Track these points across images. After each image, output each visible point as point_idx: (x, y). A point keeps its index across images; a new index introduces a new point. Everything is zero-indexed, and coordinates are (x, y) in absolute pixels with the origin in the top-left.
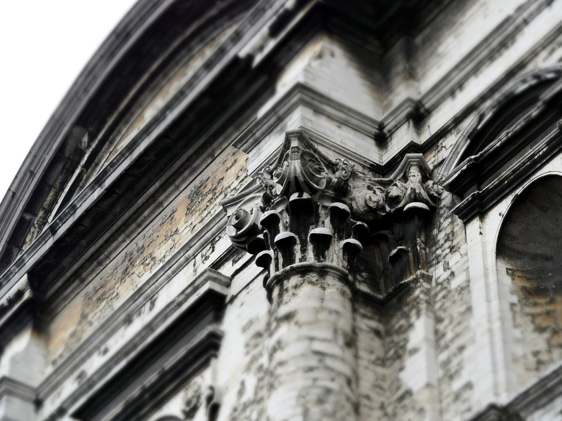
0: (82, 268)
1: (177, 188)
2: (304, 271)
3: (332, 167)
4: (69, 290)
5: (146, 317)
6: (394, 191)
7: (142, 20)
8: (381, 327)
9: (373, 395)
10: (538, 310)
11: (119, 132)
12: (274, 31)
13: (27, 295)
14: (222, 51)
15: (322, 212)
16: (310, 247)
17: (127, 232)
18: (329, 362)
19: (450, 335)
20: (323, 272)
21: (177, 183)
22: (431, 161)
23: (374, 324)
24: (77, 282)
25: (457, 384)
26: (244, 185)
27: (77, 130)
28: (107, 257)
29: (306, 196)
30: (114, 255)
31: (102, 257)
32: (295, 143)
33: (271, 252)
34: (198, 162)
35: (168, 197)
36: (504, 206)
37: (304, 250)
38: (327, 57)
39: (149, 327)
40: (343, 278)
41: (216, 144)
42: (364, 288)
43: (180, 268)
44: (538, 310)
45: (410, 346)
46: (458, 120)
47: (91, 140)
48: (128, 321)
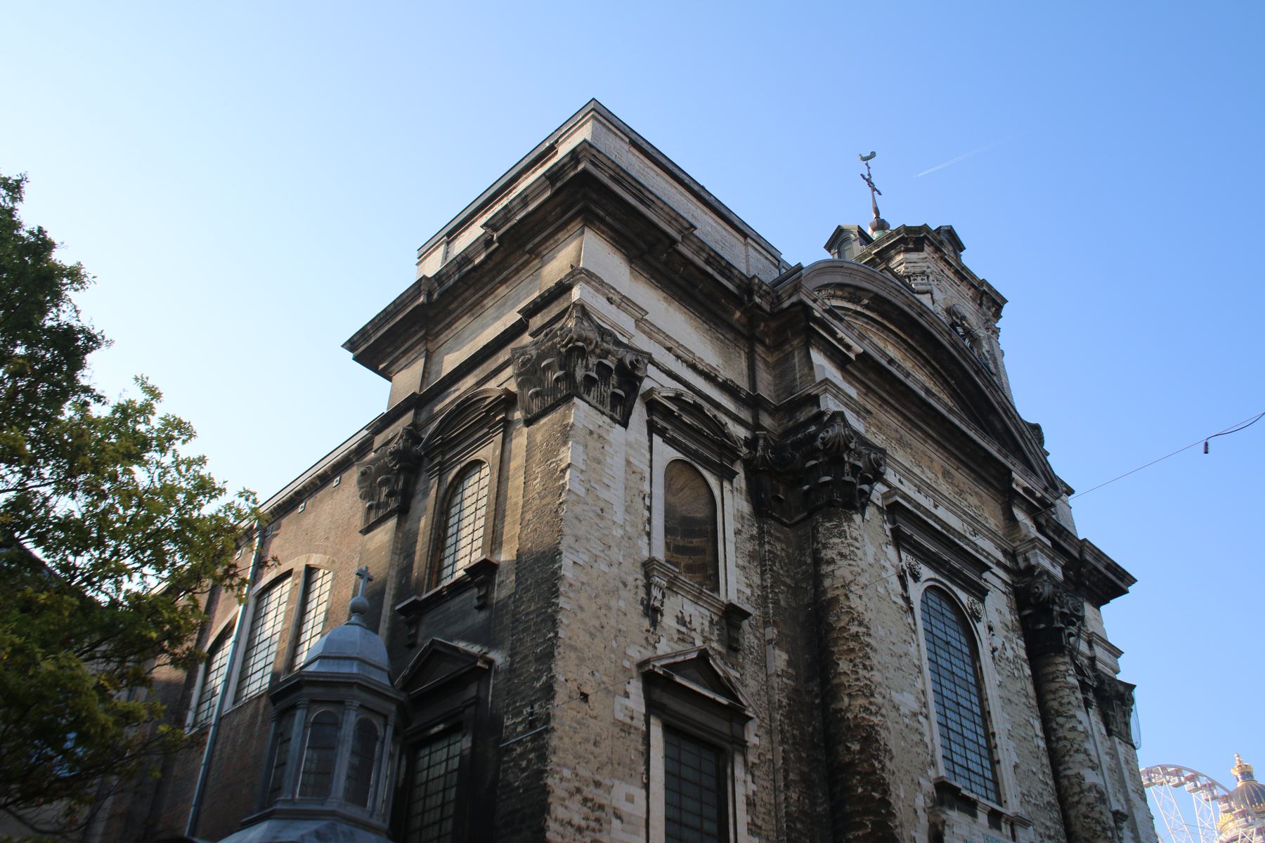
0: (875, 392)
1: (937, 451)
4: (857, 385)
5: (927, 503)
11: (980, 484)
12: (1025, 489)
17: (905, 422)
21: (940, 450)
24: (864, 390)
26: (1102, 743)
28: (886, 411)
30: (888, 415)
31: (886, 407)
34: (953, 460)
35: (931, 446)
41: (964, 469)
43: (711, 276)
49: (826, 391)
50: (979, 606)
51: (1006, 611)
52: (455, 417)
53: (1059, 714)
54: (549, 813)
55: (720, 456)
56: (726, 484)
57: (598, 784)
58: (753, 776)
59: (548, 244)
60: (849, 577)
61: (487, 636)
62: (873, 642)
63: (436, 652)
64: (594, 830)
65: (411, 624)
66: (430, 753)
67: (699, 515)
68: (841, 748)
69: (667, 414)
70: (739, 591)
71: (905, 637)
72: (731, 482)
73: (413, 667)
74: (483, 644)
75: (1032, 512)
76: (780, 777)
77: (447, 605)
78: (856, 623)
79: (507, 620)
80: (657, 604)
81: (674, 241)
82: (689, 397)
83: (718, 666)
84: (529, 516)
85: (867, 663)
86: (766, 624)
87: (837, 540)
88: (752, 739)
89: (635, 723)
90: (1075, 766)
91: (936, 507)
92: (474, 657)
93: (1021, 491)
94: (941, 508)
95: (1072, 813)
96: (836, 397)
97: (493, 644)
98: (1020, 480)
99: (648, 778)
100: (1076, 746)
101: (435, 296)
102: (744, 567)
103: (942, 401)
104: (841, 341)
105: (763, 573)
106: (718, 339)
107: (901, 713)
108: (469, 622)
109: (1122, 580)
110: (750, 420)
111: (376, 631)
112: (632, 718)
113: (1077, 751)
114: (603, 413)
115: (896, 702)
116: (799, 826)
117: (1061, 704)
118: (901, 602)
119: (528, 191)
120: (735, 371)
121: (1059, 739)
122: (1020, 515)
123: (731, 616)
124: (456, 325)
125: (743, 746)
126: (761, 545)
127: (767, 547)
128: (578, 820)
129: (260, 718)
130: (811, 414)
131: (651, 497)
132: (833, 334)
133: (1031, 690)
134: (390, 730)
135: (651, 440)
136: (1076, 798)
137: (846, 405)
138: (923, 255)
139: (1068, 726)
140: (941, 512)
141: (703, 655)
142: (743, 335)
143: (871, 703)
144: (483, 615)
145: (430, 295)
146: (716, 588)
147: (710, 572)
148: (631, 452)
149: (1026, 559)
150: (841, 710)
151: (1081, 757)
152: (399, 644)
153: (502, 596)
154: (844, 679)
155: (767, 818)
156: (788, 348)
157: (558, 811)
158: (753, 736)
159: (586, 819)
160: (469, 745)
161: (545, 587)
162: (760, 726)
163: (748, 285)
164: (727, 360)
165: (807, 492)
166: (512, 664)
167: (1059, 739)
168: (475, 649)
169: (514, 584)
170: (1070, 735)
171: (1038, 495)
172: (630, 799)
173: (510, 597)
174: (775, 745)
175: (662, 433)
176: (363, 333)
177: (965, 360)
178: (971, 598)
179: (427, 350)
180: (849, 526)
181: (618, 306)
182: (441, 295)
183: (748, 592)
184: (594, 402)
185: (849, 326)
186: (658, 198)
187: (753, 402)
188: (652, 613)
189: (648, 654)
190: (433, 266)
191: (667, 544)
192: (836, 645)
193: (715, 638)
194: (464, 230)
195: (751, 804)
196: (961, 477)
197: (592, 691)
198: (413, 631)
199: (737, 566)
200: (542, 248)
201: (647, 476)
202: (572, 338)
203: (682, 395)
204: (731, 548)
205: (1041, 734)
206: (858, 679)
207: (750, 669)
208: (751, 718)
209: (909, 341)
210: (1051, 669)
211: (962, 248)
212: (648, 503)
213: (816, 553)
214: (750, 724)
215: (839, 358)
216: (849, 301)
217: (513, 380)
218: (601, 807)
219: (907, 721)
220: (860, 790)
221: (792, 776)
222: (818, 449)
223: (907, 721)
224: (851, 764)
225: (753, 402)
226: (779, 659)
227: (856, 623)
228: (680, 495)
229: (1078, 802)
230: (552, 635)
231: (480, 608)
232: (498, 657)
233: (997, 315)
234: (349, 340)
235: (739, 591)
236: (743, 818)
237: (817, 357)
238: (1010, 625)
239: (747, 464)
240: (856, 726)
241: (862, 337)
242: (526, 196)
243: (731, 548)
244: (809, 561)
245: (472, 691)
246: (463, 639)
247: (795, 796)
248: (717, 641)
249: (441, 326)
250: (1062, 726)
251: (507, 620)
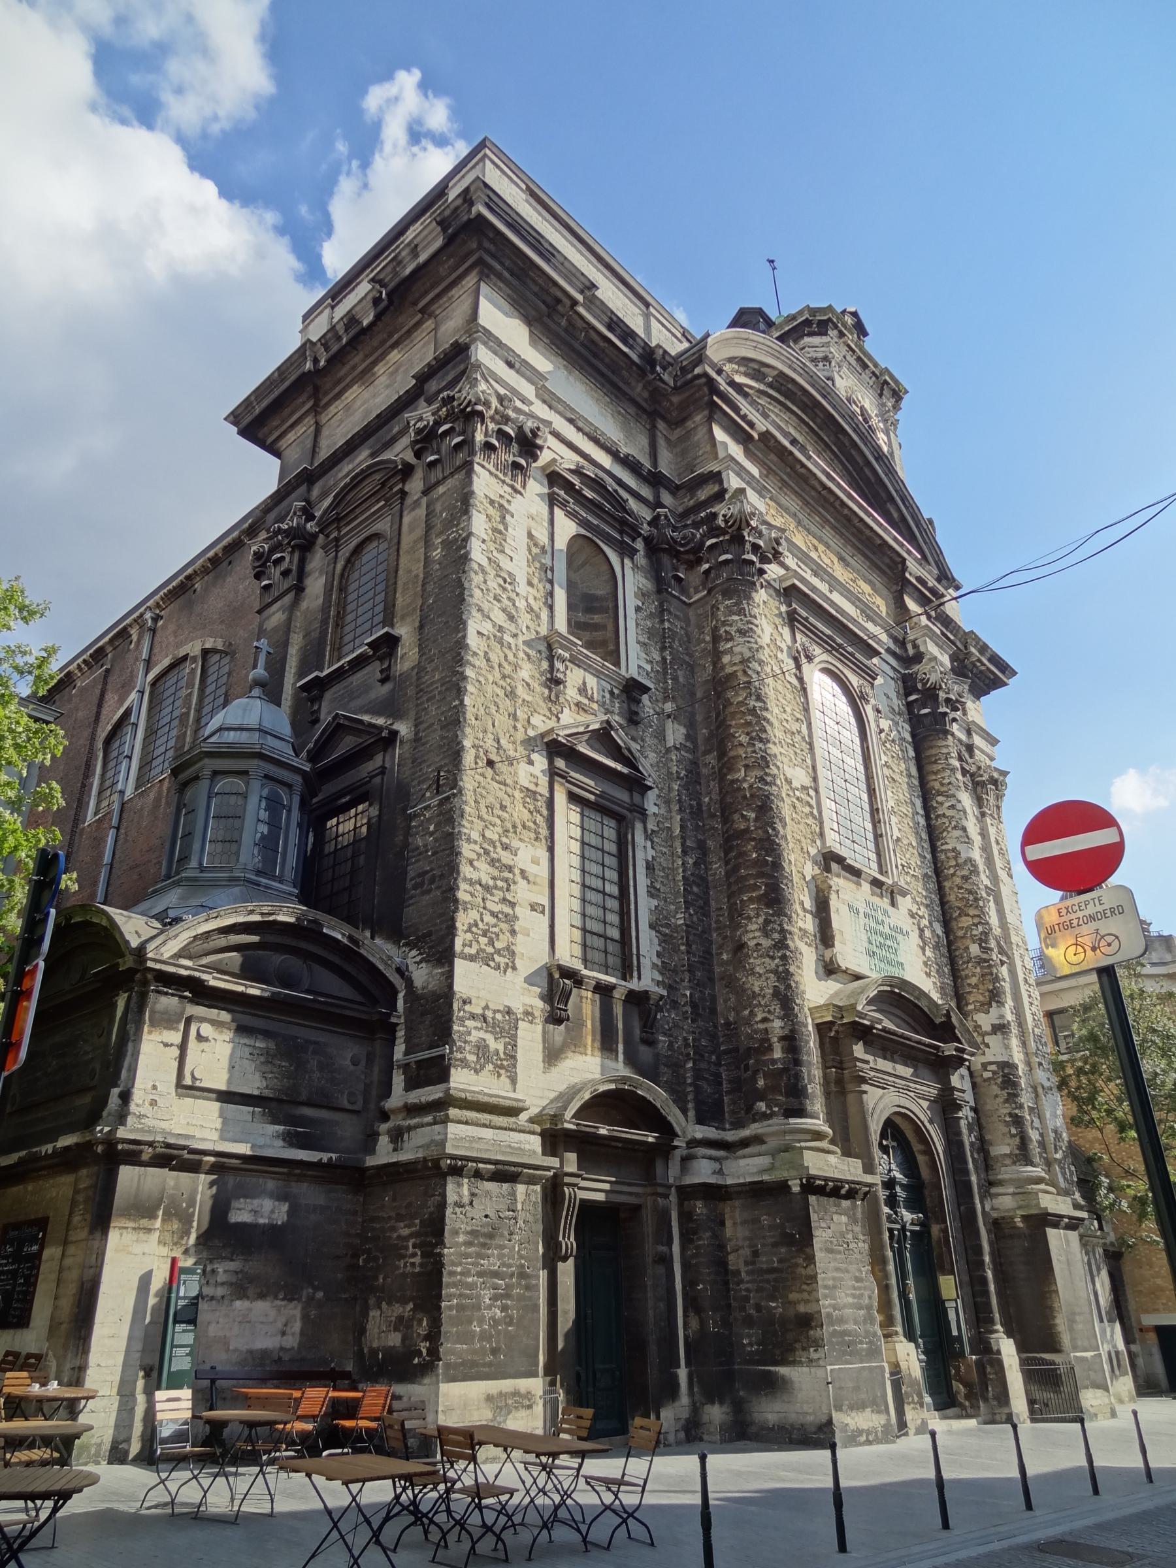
5: (823, 587)
12: (919, 579)
49: (728, 468)
50: (868, 690)
51: (893, 695)
52: (351, 490)
53: (939, 793)
54: (458, 873)
55: (621, 532)
56: (627, 561)
57: (506, 847)
58: (652, 842)
59: (441, 302)
60: (748, 654)
61: (391, 707)
62: (769, 716)
63: (339, 726)
64: (501, 889)
65: (313, 700)
66: (338, 824)
67: (600, 592)
68: (736, 817)
69: (569, 487)
70: (639, 667)
71: (799, 716)
72: (632, 559)
73: (317, 741)
74: (388, 717)
75: (923, 601)
76: (678, 844)
77: (350, 679)
78: (754, 697)
79: (411, 691)
80: (560, 676)
81: (575, 302)
82: (590, 472)
83: (620, 737)
84: (429, 588)
85: (764, 736)
86: (666, 699)
87: (736, 618)
88: (651, 809)
89: (539, 789)
90: (951, 841)
91: (831, 592)
92: (380, 729)
93: (914, 581)
94: (835, 593)
95: (947, 884)
96: (738, 475)
97: (397, 715)
98: (914, 569)
99: (553, 842)
100: (953, 823)
101: (322, 363)
102: (645, 644)
103: (841, 487)
104: (744, 417)
105: (663, 649)
106: (619, 413)
107: (793, 786)
108: (373, 695)
109: (1003, 672)
110: (651, 498)
111: (279, 704)
112: (537, 785)
113: (955, 827)
114: (504, 482)
115: (789, 776)
116: (695, 889)
117: (942, 785)
118: (795, 682)
119: (418, 239)
120: (635, 448)
121: (938, 816)
122: (912, 606)
123: (632, 690)
124: (346, 395)
125: (643, 813)
126: (662, 621)
127: (667, 625)
128: (486, 879)
129: (163, 800)
130: (712, 492)
131: (552, 570)
132: (737, 410)
133: (914, 771)
134: (296, 799)
135: (552, 513)
136: (952, 871)
137: (748, 483)
138: (825, 339)
139: (947, 804)
140: (836, 597)
141: (607, 727)
142: (644, 410)
143: (766, 774)
144: (388, 687)
145: (316, 361)
146: (617, 664)
147: (612, 647)
148: (533, 524)
149: (915, 646)
150: (737, 780)
151: (957, 833)
152: (303, 719)
153: (405, 669)
154: (741, 751)
155: (665, 881)
156: (690, 424)
157: (466, 870)
158: (651, 804)
159: (494, 878)
160: (377, 813)
161: (448, 656)
162: (659, 796)
163: (650, 356)
164: (628, 434)
165: (707, 572)
166: (416, 734)
167: (938, 816)
168: (380, 721)
169: (417, 656)
170: (949, 813)
171: (930, 584)
172: (535, 861)
173: (413, 668)
174: (673, 814)
175: (563, 505)
176: (247, 403)
177: (866, 444)
178: (861, 682)
179: (317, 423)
180: (748, 604)
181: (518, 372)
182: (328, 361)
183: (648, 667)
184: (493, 470)
185: (753, 403)
186: (559, 252)
187: (655, 480)
188: (554, 682)
189: (552, 724)
190: (318, 330)
191: (569, 621)
192: (733, 718)
193: (617, 711)
194: (349, 293)
195: (650, 867)
196: (856, 561)
197: (499, 759)
198: (316, 708)
199: (638, 642)
200: (436, 305)
201: (549, 549)
202: (470, 401)
203: (583, 467)
204: (631, 625)
205: (921, 812)
206: (754, 752)
207: (650, 741)
208: (650, 788)
209: (811, 423)
210: (933, 752)
211: (865, 334)
212: (550, 576)
213: (715, 630)
214: (649, 793)
215: (742, 436)
216: (753, 378)
217: (410, 450)
218: (510, 869)
219: (797, 793)
220: (754, 855)
221: (689, 843)
222: (719, 528)
223: (797, 793)
224: (747, 831)
225: (655, 480)
226: (675, 733)
227: (754, 697)
228: (582, 571)
229: (953, 875)
230: (457, 702)
231: (383, 681)
232: (403, 729)
233: (896, 407)
234: (232, 413)
235: (639, 667)
236: (643, 881)
237: (719, 434)
238: (897, 709)
239: (648, 541)
240: (752, 795)
241: (765, 416)
242: (416, 246)
243: (631, 625)
244: (708, 638)
245: (378, 760)
246: (367, 712)
247: (691, 861)
248: (618, 714)
249: (331, 395)
250: (941, 804)
251: (411, 691)
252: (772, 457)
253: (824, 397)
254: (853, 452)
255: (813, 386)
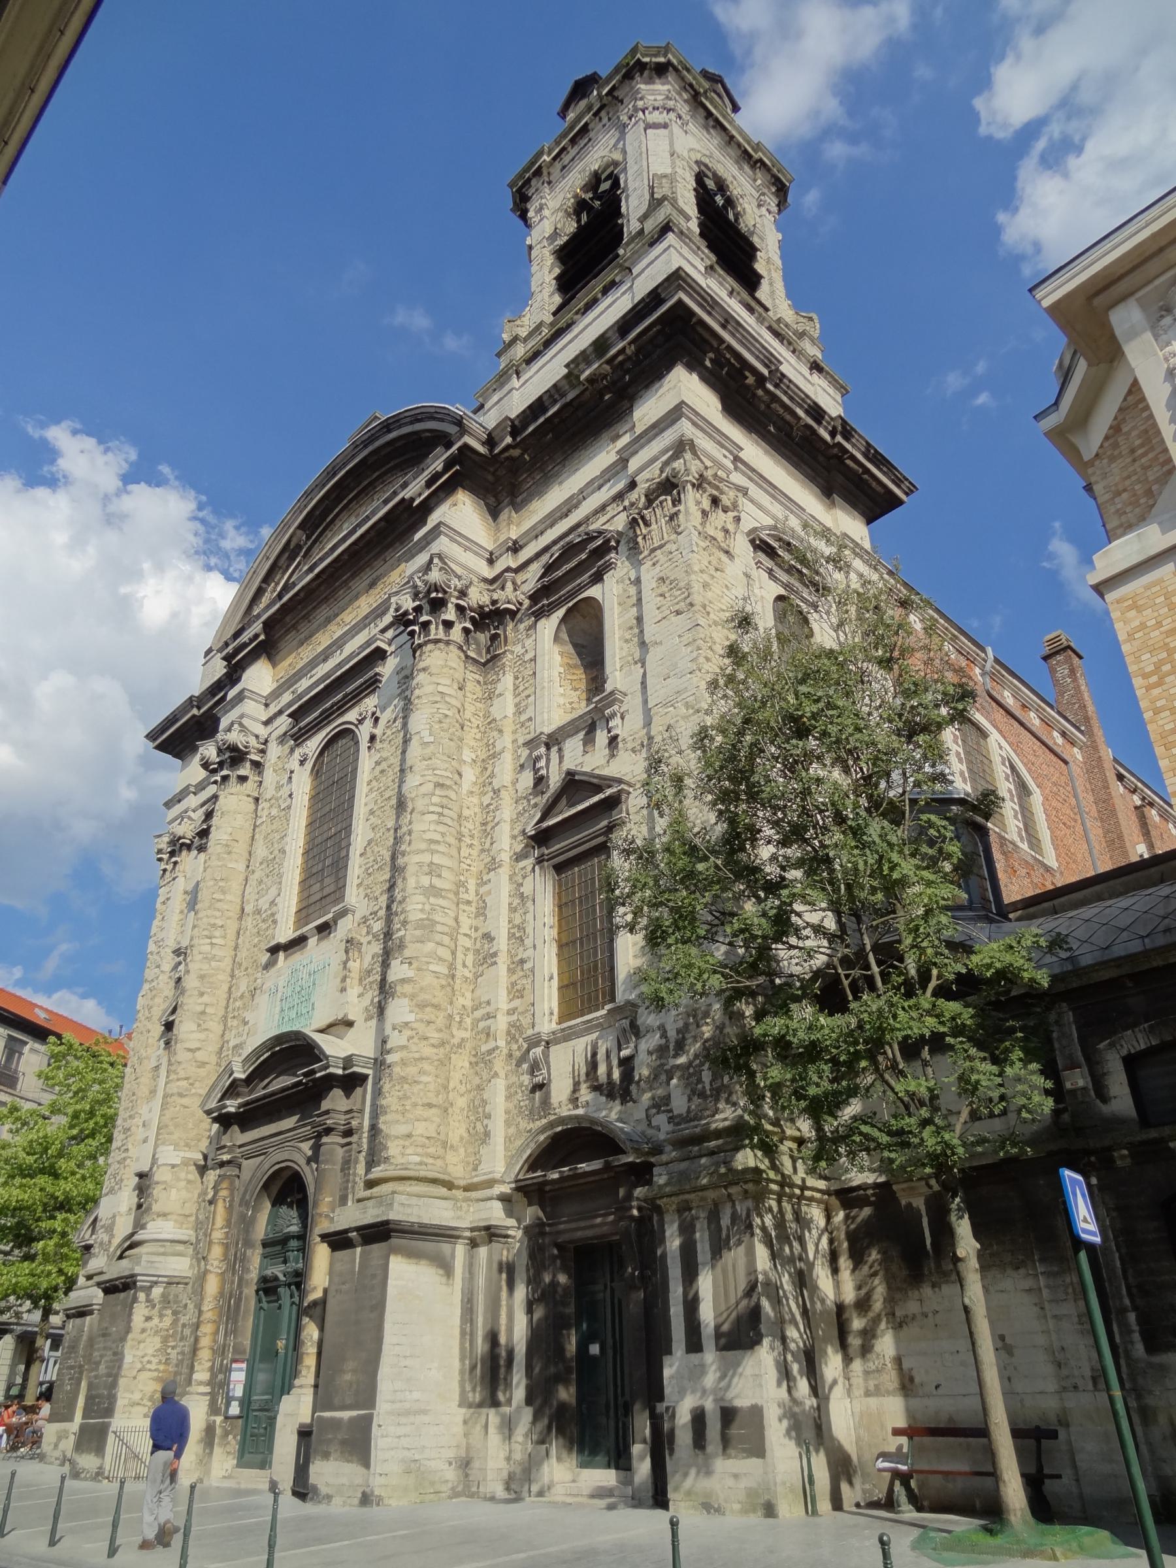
2: (437, 641)
3: (459, 578)
6: (495, 597)
7: (345, 465)
8: (481, 679)
9: (473, 720)
10: (575, 677)
12: (429, 484)
13: (262, 637)
14: (395, 493)
15: (450, 605)
16: (441, 627)
18: (447, 699)
19: (521, 688)
20: (448, 643)
22: (520, 578)
23: (477, 677)
25: (524, 717)
27: (300, 532)
29: (440, 595)
32: (436, 561)
33: (416, 628)
36: (561, 612)
37: (437, 629)
38: (460, 505)
39: (340, 666)
40: (460, 648)
42: (472, 654)
44: (575, 677)
45: (497, 692)
46: (538, 555)
47: (308, 538)
48: (325, 660)
104: (252, 640)
132: (245, 645)
252: (288, 619)
253: (335, 475)
254: (383, 453)
255: (324, 485)
